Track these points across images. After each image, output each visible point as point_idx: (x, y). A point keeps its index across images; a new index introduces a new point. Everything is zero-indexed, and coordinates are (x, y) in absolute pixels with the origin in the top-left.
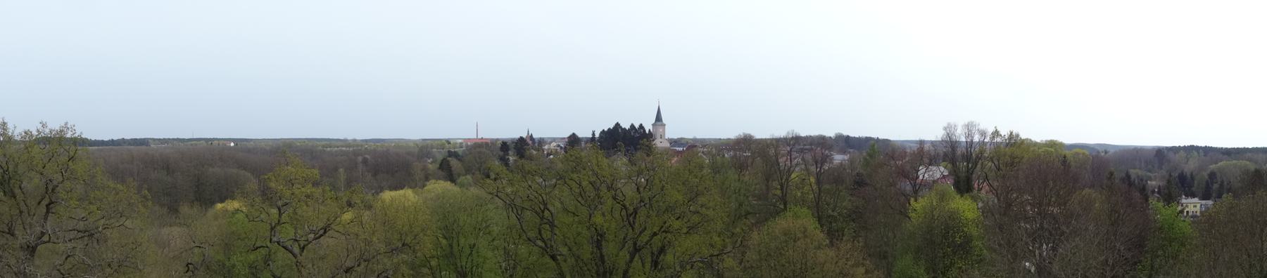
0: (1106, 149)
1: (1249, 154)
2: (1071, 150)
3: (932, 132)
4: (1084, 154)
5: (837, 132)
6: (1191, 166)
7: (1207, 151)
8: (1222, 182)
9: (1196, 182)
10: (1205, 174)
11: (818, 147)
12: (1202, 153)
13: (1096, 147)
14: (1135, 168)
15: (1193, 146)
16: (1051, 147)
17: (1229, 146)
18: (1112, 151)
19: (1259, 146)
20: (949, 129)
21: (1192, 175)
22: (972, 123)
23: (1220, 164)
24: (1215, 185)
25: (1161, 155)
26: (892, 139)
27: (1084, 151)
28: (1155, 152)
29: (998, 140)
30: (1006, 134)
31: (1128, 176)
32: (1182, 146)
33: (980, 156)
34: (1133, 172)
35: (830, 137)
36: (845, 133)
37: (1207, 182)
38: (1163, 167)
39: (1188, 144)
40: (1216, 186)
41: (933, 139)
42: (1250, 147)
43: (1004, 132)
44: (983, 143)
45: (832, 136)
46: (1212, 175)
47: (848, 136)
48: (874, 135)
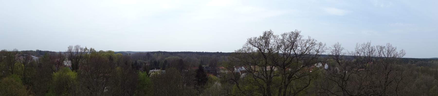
0: (130, 53)
1: (179, 54)
2: (116, 54)
3: (64, 49)
4: (121, 55)
5: (37, 49)
6: (159, 58)
7: (165, 53)
8: (169, 64)
9: (160, 64)
10: (163, 61)
11: (27, 54)
12: (163, 54)
13: (127, 53)
14: (140, 60)
15: (160, 51)
16: (110, 53)
17: (171, 51)
18: (132, 54)
19: (183, 51)
20: (70, 48)
21: (159, 61)
22: (78, 45)
23: (169, 57)
24: (167, 65)
25: (149, 55)
26: (56, 51)
27: (121, 54)
28: (146, 54)
29: (87, 51)
30: (89, 49)
31: (136, 63)
32: (156, 51)
33: (81, 57)
34: (138, 61)
35: (35, 51)
36: (40, 50)
37: (164, 64)
38: (149, 59)
39: (158, 51)
40: (167, 65)
41: (65, 51)
42: (180, 52)
43: (89, 48)
44: (81, 53)
45: (35, 51)
46: (166, 61)
47: (41, 51)
48: (50, 50)
